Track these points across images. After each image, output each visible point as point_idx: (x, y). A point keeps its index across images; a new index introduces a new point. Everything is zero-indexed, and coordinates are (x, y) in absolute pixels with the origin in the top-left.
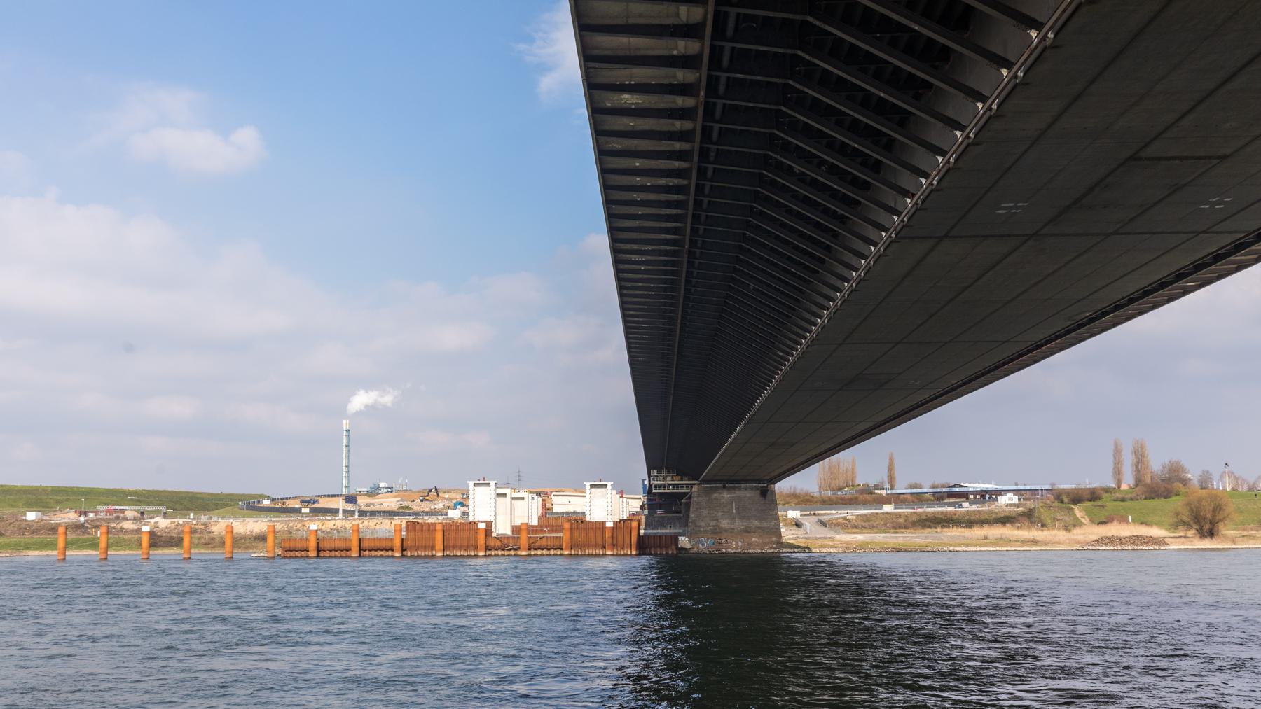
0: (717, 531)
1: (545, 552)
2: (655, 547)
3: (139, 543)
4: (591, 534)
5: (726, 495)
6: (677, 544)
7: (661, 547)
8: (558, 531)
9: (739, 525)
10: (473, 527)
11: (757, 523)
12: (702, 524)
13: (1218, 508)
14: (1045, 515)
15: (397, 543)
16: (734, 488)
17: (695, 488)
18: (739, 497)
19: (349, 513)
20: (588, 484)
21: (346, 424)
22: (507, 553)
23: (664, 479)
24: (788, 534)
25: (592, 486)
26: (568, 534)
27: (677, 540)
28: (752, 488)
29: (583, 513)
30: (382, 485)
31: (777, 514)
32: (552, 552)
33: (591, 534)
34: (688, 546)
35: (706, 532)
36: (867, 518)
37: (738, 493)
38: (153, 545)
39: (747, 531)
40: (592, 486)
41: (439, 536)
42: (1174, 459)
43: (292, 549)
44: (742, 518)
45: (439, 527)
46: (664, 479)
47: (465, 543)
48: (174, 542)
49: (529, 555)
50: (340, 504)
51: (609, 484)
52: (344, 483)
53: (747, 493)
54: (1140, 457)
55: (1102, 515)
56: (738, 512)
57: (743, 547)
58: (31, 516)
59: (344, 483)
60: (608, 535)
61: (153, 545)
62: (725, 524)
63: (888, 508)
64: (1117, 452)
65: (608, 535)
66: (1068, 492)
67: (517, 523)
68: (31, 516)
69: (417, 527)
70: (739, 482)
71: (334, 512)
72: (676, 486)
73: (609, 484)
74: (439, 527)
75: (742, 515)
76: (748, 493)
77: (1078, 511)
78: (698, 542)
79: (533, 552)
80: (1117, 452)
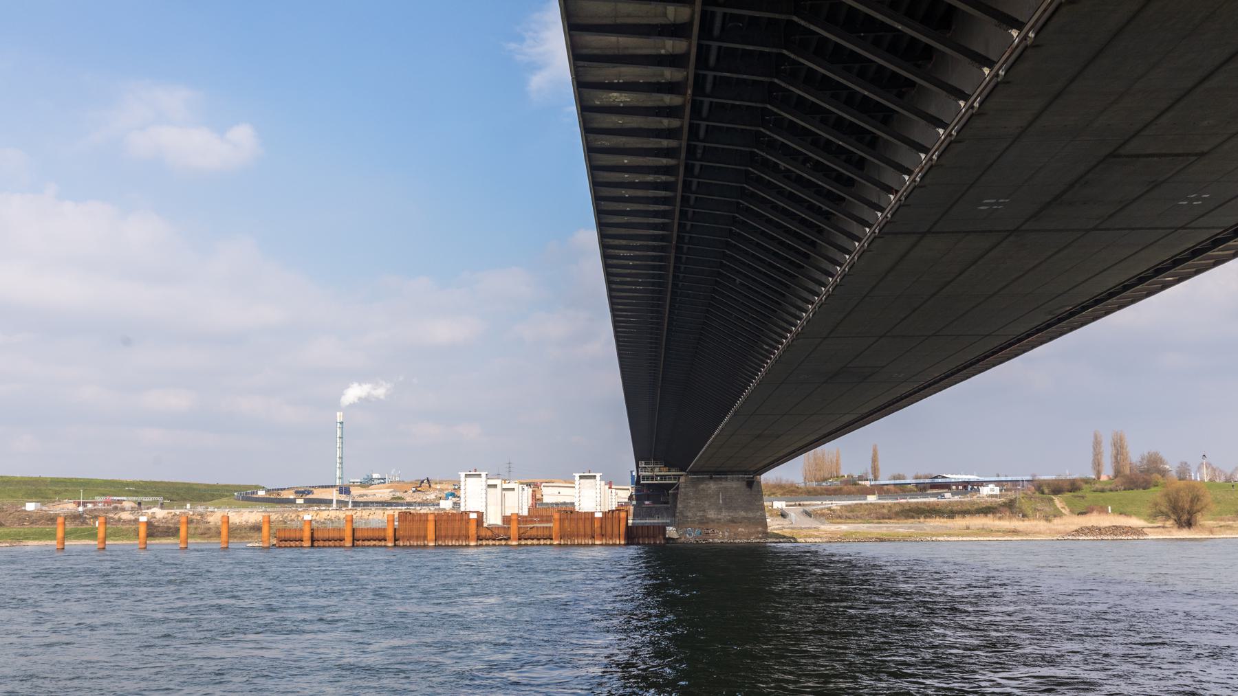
0: (704, 521)
1: (535, 542)
2: (643, 537)
3: (137, 533)
4: (581, 525)
5: (713, 486)
6: (664, 534)
7: (649, 537)
8: (548, 522)
9: (725, 515)
10: (465, 517)
11: (743, 514)
12: (690, 514)
13: (1195, 499)
14: (1026, 505)
15: (390, 533)
16: (720, 479)
17: (682, 479)
18: (726, 488)
19: (342, 504)
20: (577, 476)
21: (339, 416)
22: (497, 543)
23: (652, 470)
24: (773, 524)
25: (581, 477)
26: (557, 524)
27: (665, 530)
28: (738, 479)
29: (573, 504)
30: (375, 476)
31: (762, 505)
32: (542, 542)
33: (581, 525)
34: (676, 536)
35: (693, 522)
36: (851, 509)
37: (725, 484)
38: (150, 535)
39: (733, 521)
40: (581, 477)
41: (431, 526)
42: (1153, 450)
43: (287, 539)
44: (729, 508)
45: (431, 518)
46: (652, 470)
47: (457, 533)
48: (171, 532)
49: (519, 545)
50: (334, 495)
51: (598, 475)
52: (338, 474)
53: (734, 484)
54: (1119, 449)
55: (1082, 505)
56: (725, 503)
57: (729, 537)
58: (30, 507)
59: (338, 474)
60: (597, 525)
61: (150, 535)
62: (711, 514)
63: (872, 499)
64: (1097, 444)
65: (597, 525)
66: (1048, 483)
67: (508, 513)
68: (30, 507)
69: (410, 517)
70: (725, 473)
71: (328, 502)
72: (663, 477)
73: (598, 475)
74: (431, 518)
75: (729, 505)
76: (735, 484)
77: (1058, 501)
78: (685, 532)
79: (523, 542)
80: (1097, 444)
